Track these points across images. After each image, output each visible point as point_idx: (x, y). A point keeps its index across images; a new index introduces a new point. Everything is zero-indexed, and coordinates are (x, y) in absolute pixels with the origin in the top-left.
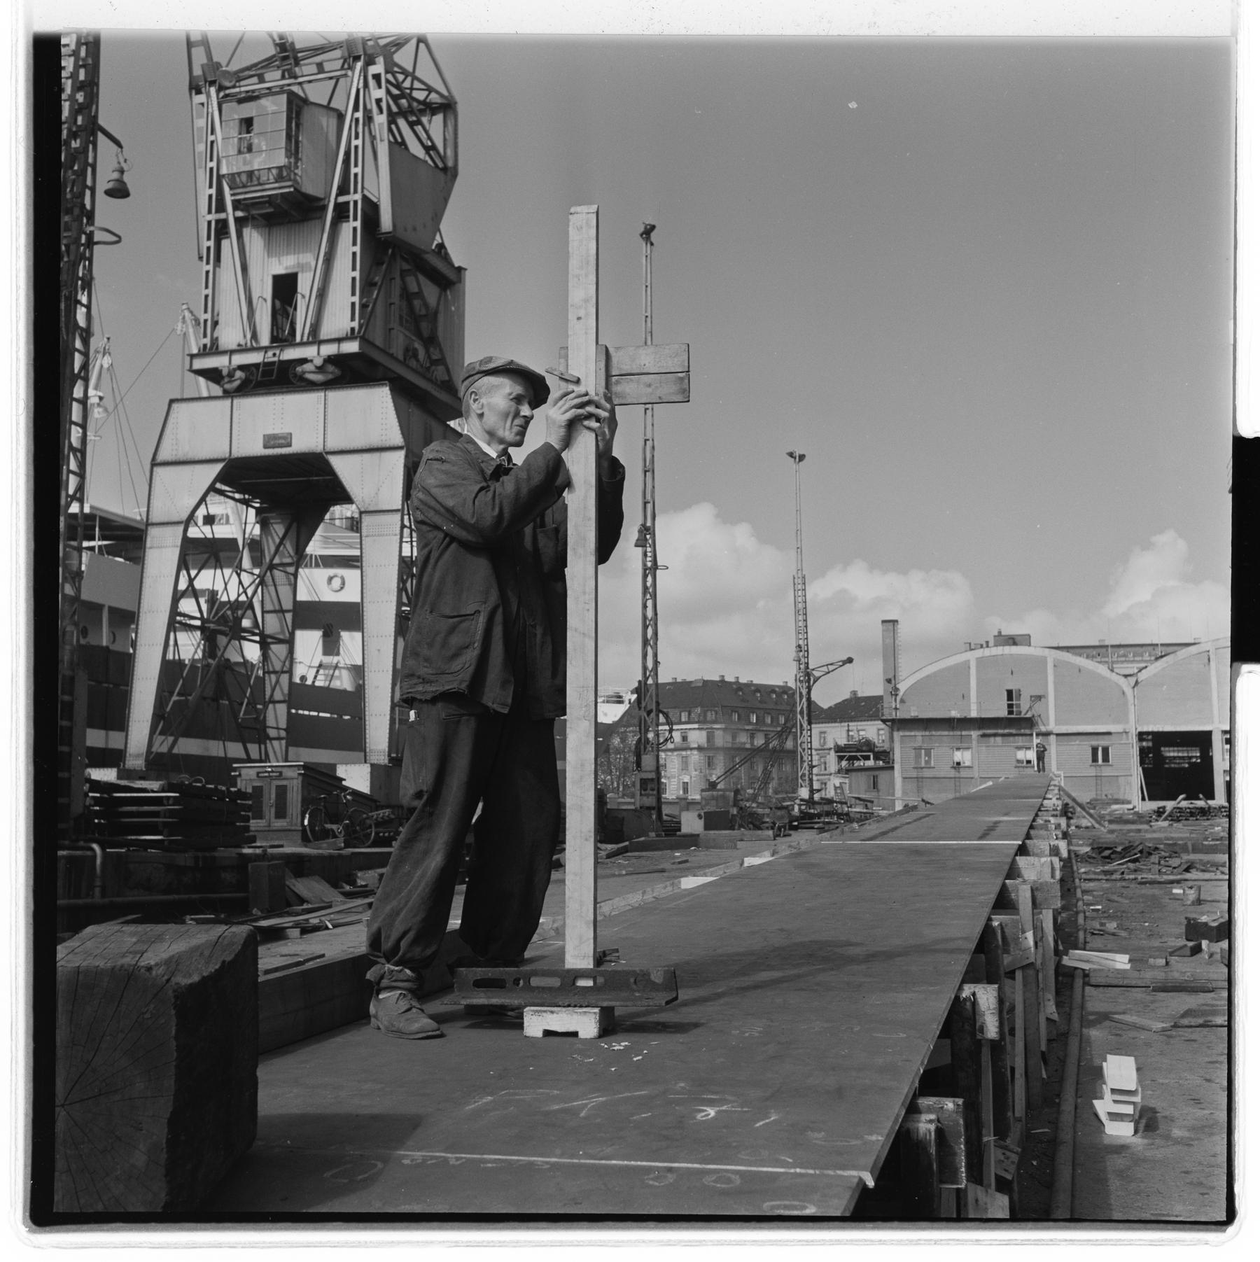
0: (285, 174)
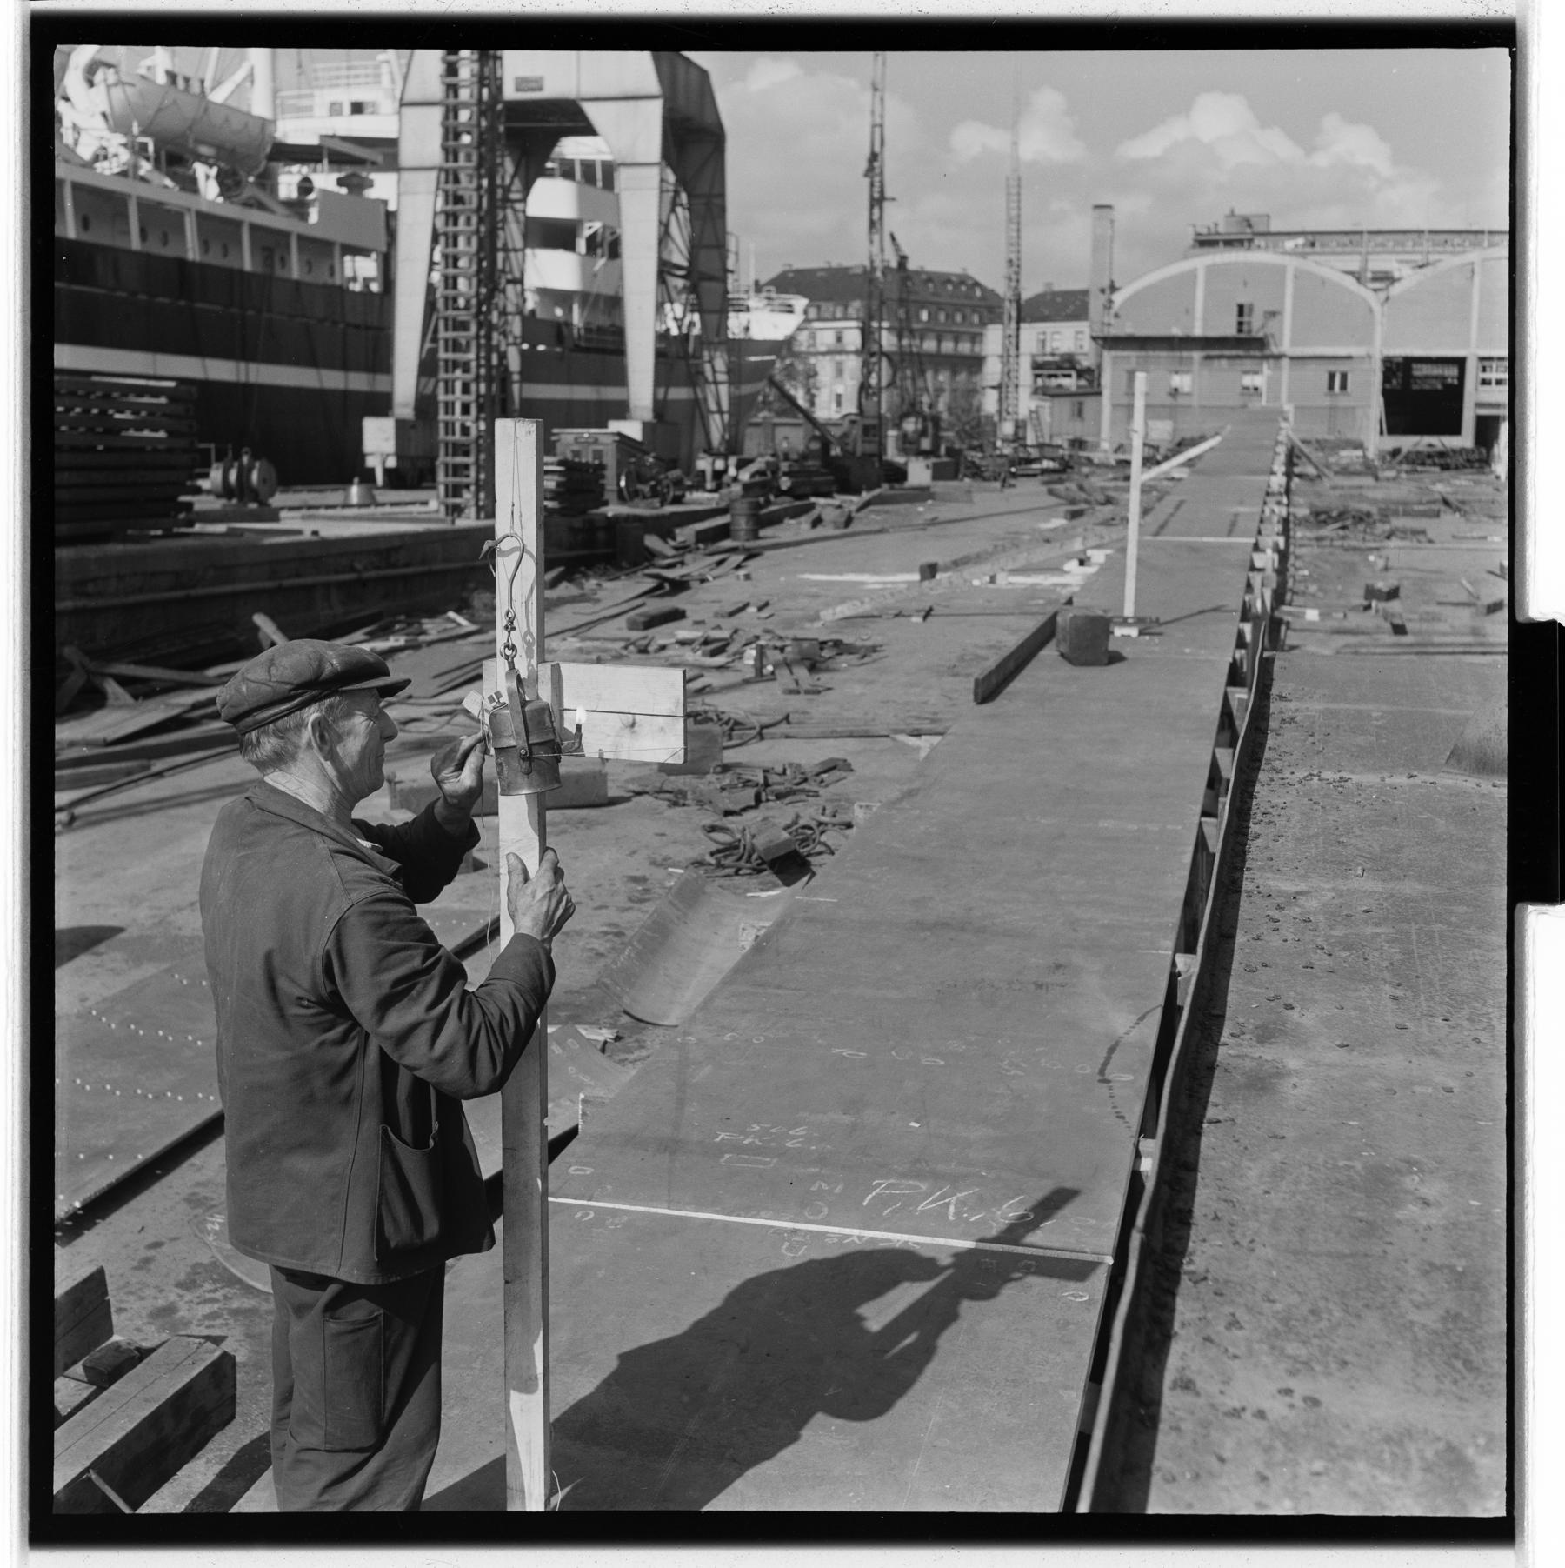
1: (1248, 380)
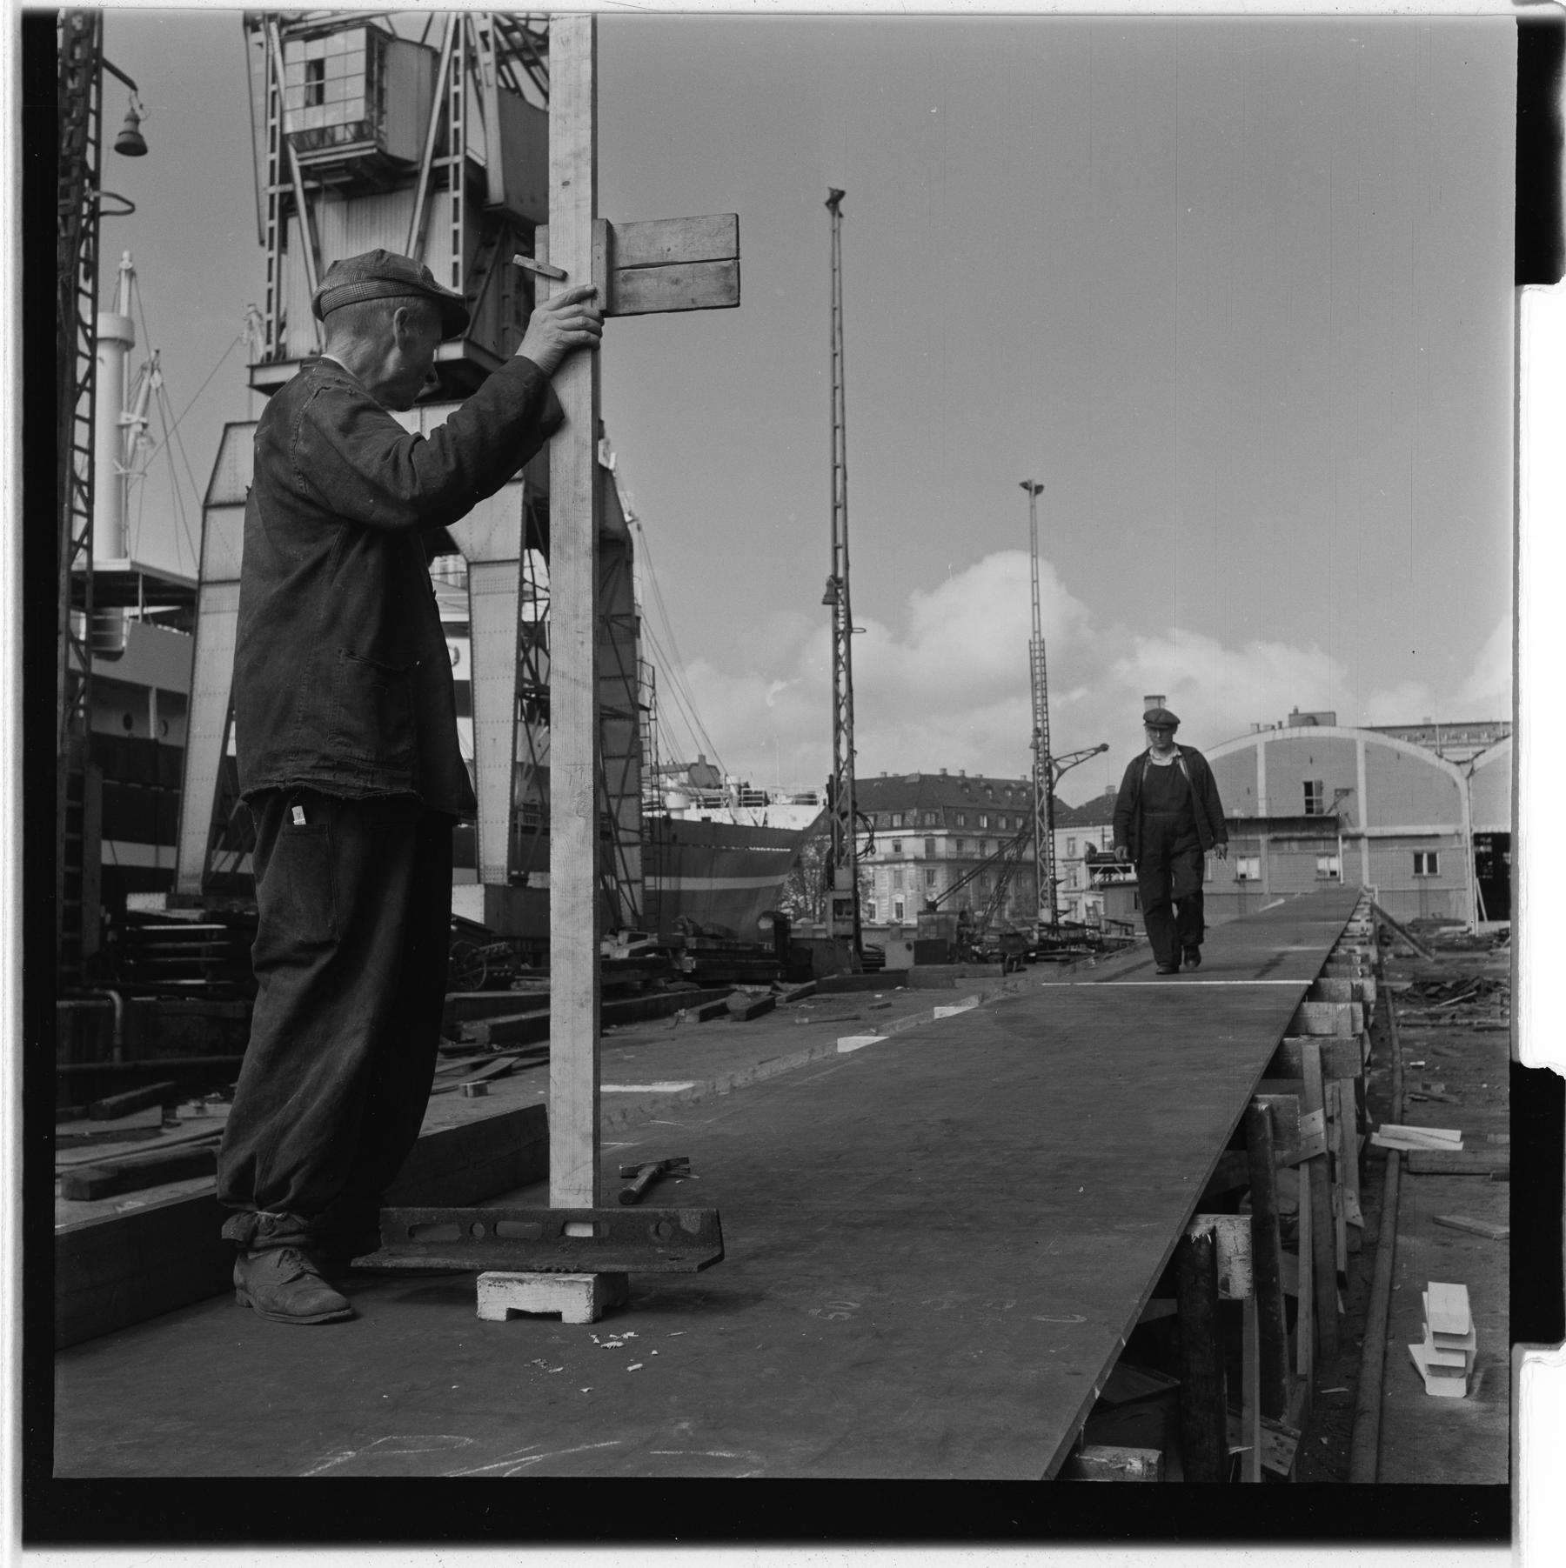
0: (366, 131)
1: (1323, 864)
